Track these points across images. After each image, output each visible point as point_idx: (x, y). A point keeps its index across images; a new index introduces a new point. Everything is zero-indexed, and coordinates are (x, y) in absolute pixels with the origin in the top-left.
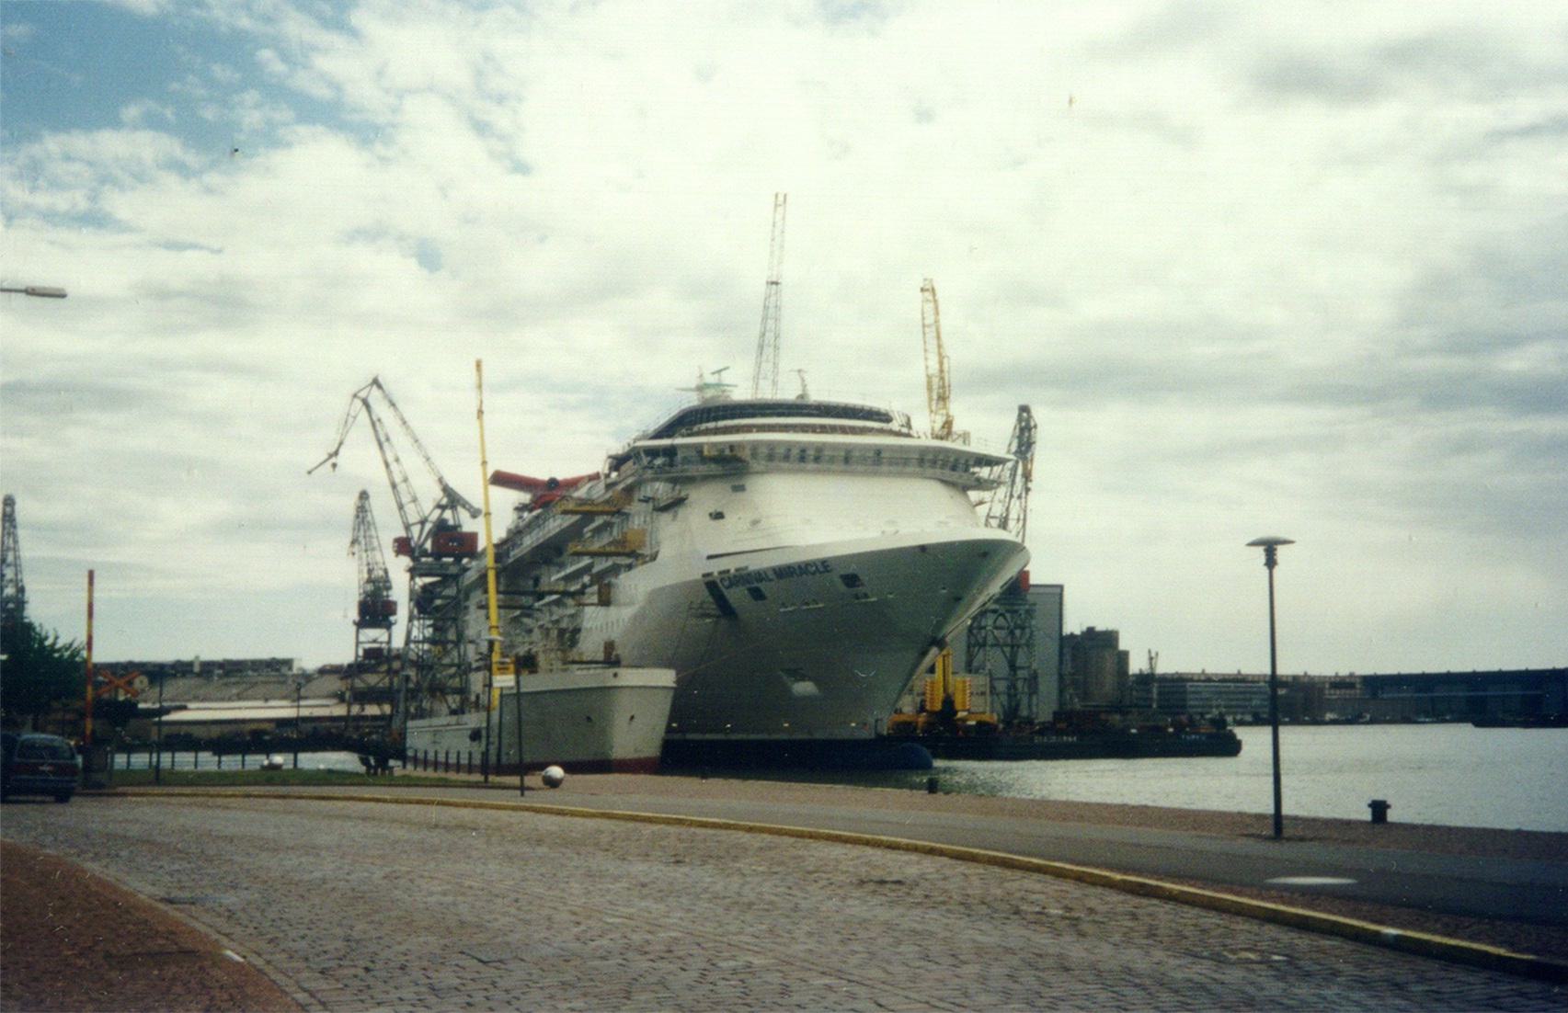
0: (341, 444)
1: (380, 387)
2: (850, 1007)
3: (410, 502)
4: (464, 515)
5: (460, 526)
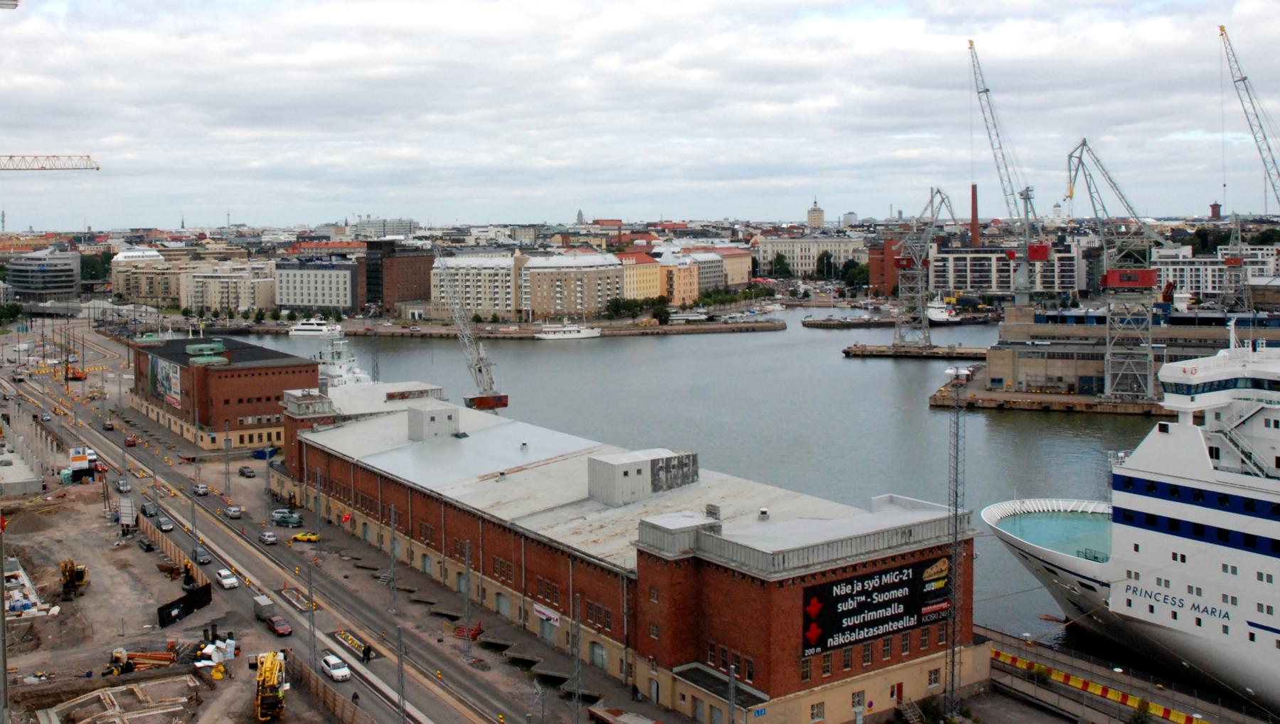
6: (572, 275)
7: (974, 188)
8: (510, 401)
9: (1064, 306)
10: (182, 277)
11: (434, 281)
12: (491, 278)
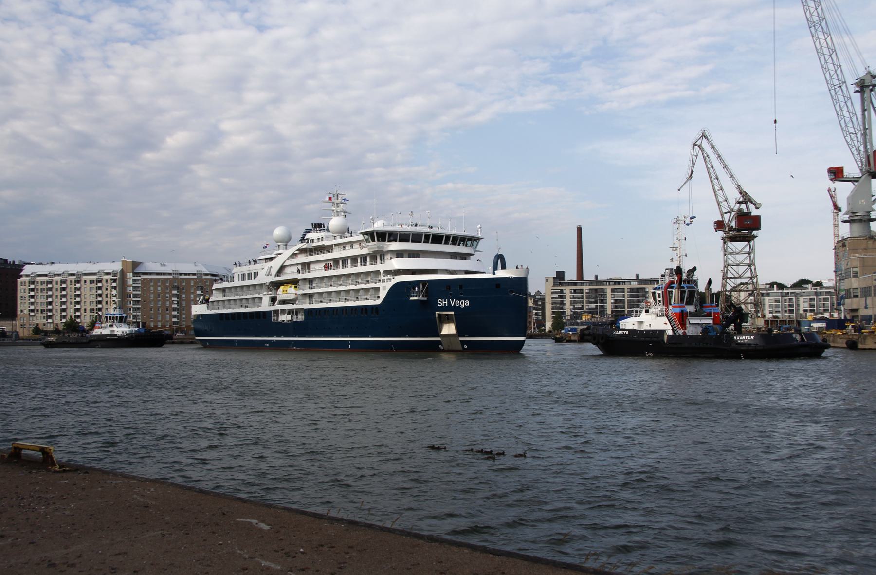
0: (692, 171)
1: (706, 137)
2: (478, 509)
3: (724, 201)
4: (752, 207)
5: (751, 213)
6: (192, 284)
7: (579, 230)
8: (596, 274)
9: (250, 278)
10: (801, 298)
11: (22, 290)
12: (43, 287)
